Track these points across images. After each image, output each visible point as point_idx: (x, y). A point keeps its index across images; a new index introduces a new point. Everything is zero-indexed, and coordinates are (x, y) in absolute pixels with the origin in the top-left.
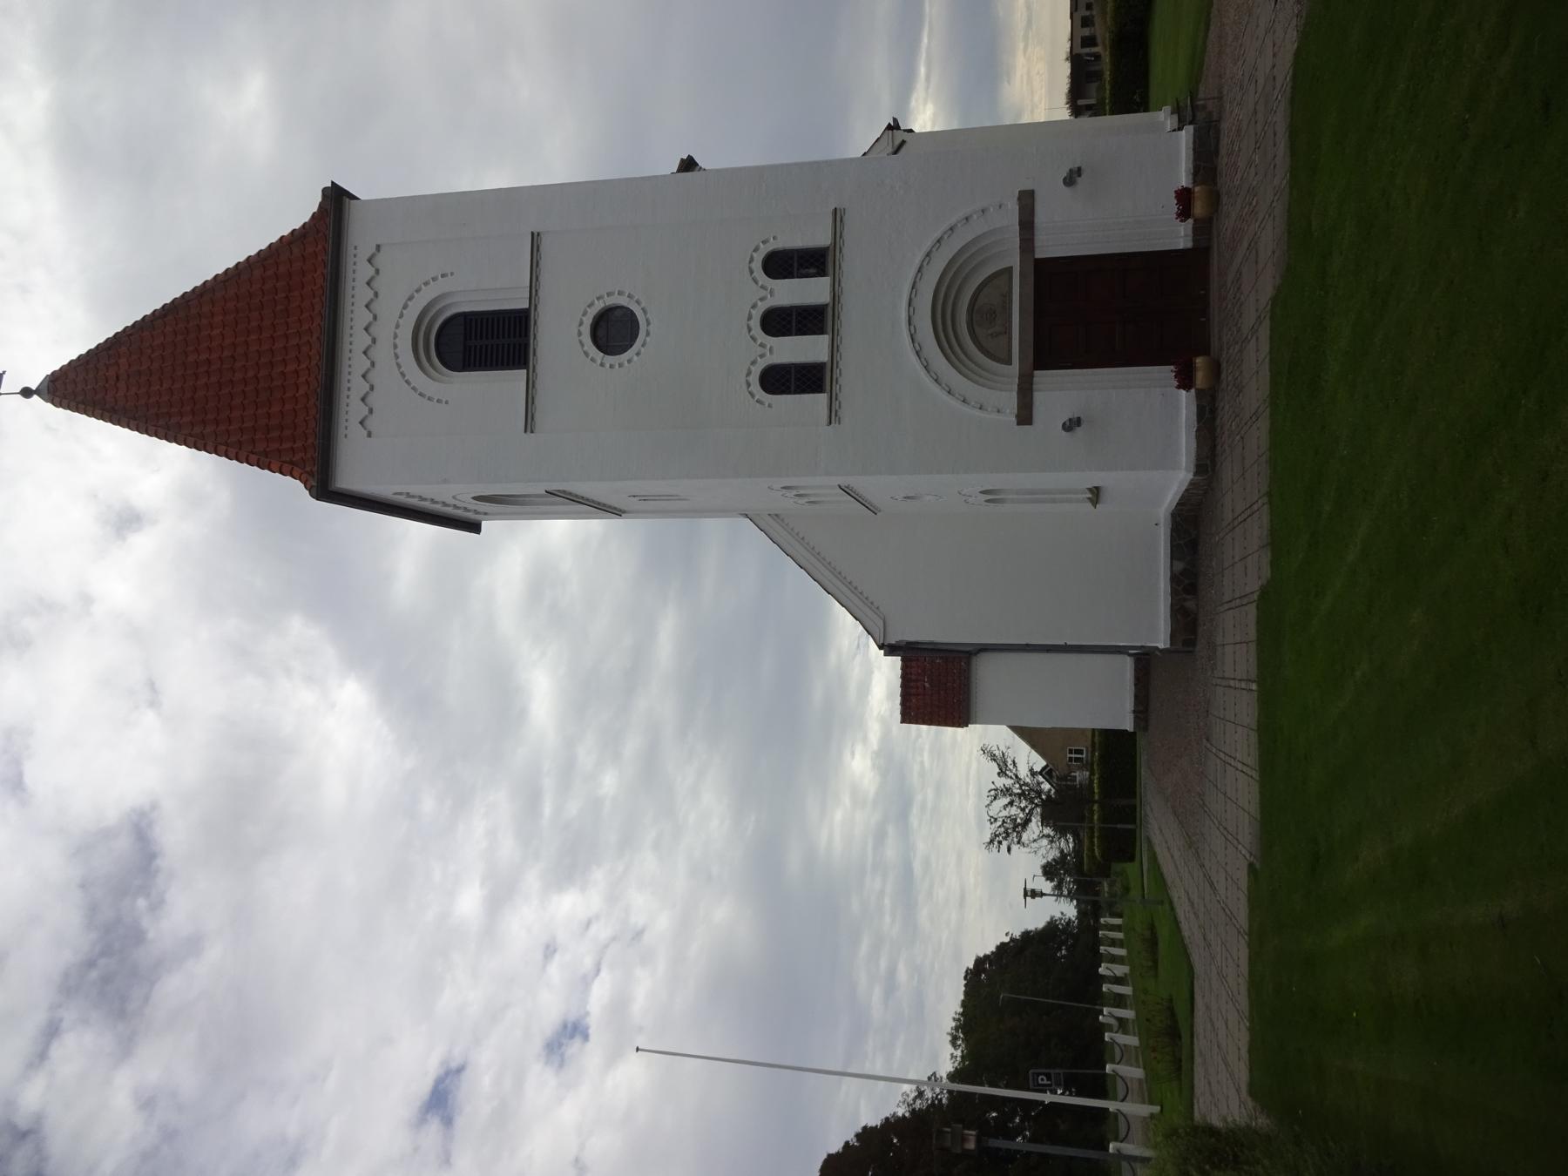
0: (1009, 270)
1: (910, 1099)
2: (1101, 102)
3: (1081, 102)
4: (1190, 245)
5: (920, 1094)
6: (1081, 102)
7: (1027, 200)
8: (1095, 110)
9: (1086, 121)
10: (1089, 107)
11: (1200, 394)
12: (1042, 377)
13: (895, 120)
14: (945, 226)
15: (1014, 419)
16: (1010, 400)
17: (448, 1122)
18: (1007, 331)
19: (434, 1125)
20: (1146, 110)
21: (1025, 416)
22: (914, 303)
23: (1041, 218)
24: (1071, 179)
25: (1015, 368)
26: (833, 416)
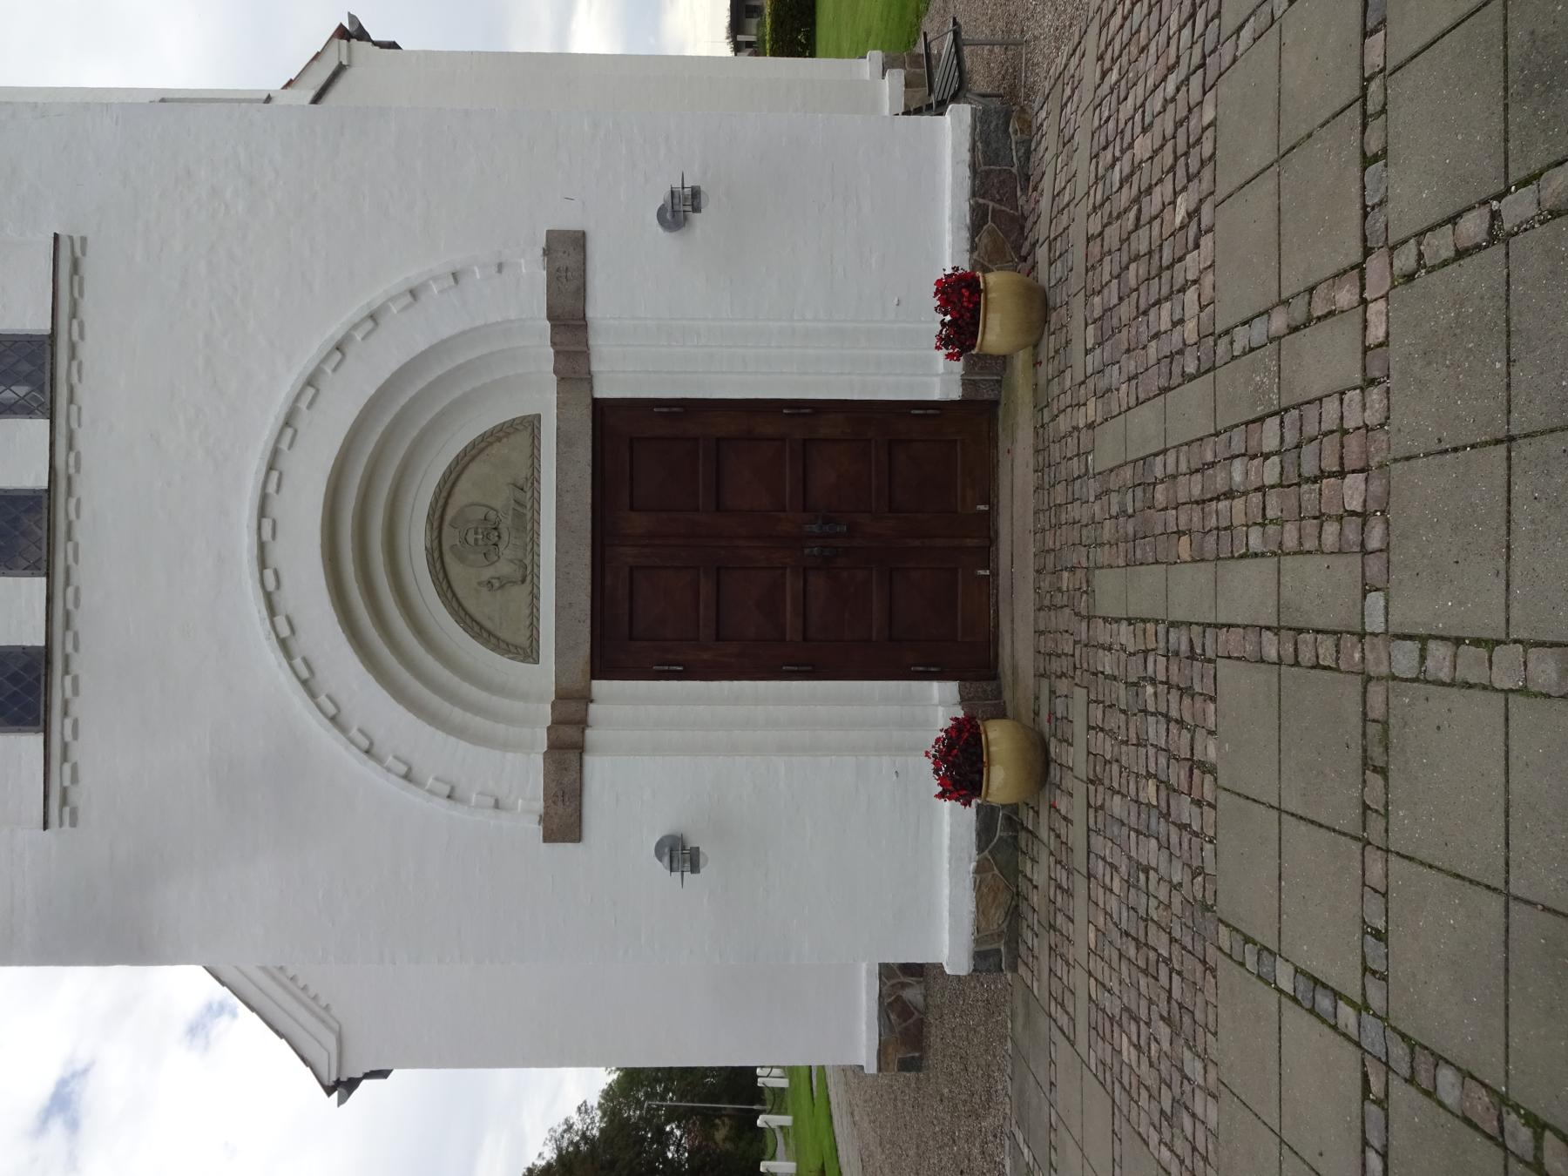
0: (530, 425)
1: (558, 1135)
2: (761, 40)
3: (740, 38)
4: (955, 394)
5: (570, 1127)
6: (740, 38)
7: (567, 257)
8: (755, 49)
9: (746, 59)
10: (749, 44)
11: (987, 819)
12: (617, 700)
13: (352, 18)
14: (355, 310)
15: (538, 831)
16: (524, 775)
17: (73, 1125)
18: (528, 574)
19: (57, 1128)
20: (812, 55)
21: (564, 819)
22: (275, 508)
23: (601, 308)
24: (680, 209)
25: (542, 676)
26: (56, 805)
